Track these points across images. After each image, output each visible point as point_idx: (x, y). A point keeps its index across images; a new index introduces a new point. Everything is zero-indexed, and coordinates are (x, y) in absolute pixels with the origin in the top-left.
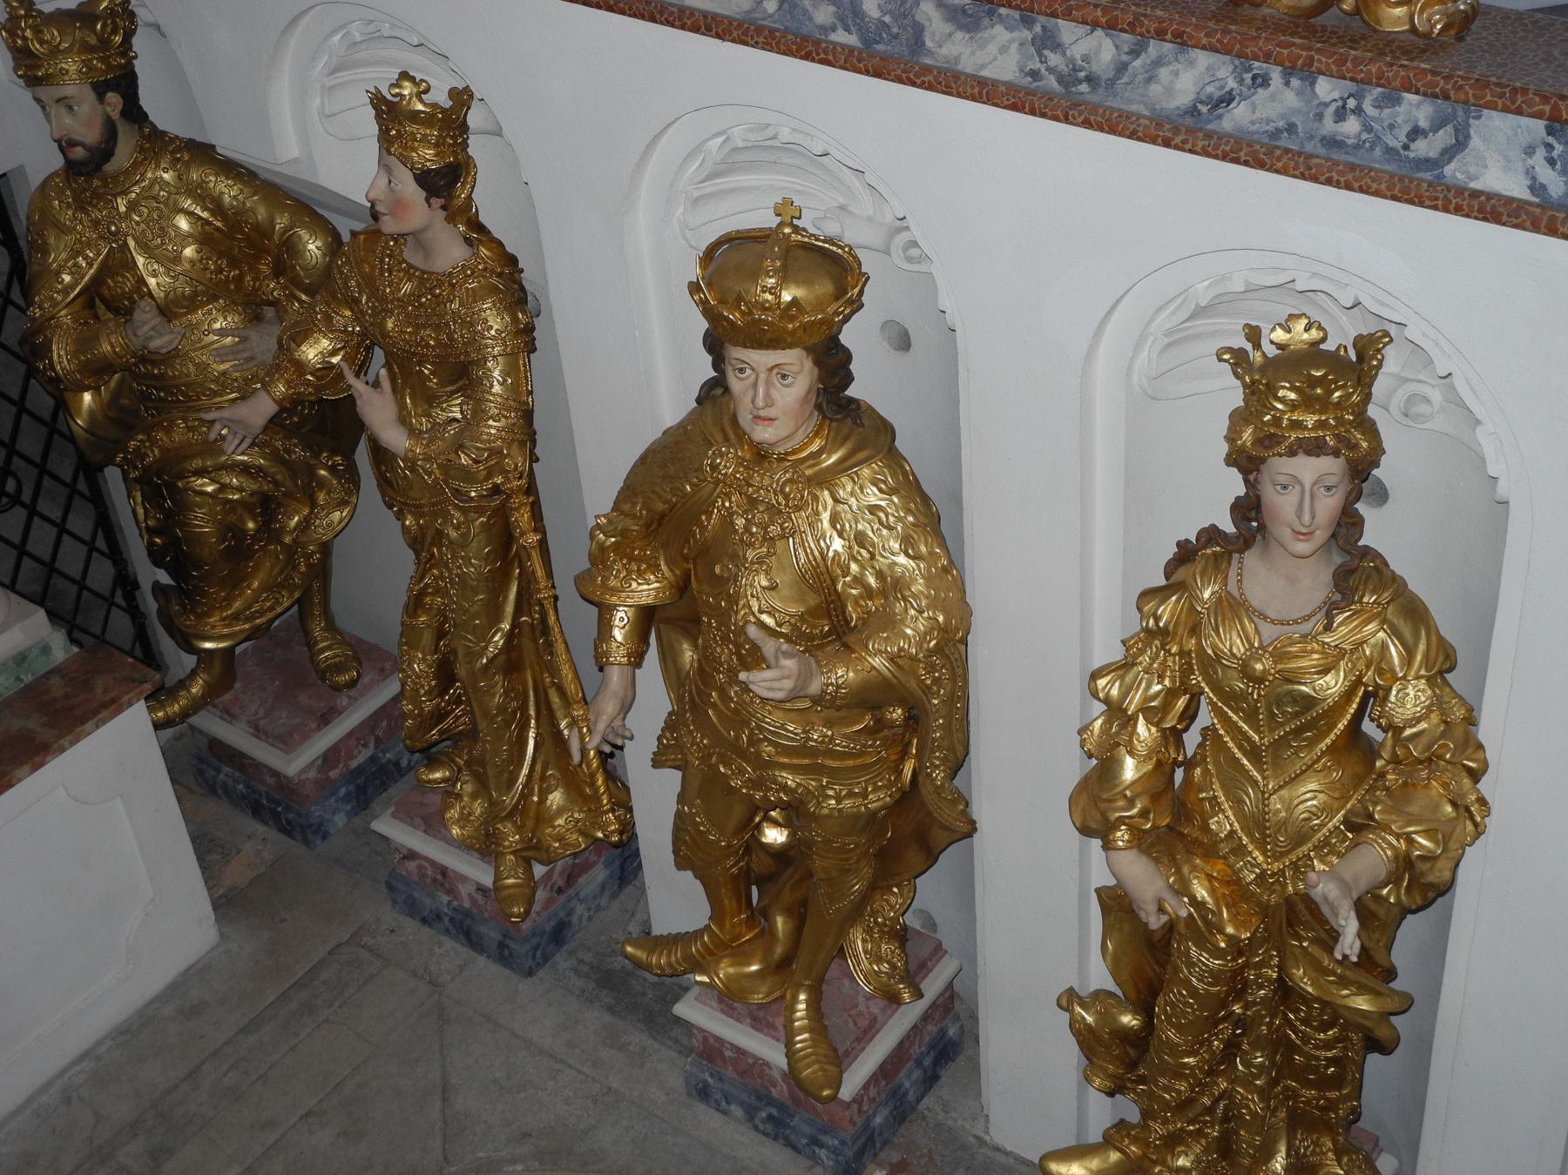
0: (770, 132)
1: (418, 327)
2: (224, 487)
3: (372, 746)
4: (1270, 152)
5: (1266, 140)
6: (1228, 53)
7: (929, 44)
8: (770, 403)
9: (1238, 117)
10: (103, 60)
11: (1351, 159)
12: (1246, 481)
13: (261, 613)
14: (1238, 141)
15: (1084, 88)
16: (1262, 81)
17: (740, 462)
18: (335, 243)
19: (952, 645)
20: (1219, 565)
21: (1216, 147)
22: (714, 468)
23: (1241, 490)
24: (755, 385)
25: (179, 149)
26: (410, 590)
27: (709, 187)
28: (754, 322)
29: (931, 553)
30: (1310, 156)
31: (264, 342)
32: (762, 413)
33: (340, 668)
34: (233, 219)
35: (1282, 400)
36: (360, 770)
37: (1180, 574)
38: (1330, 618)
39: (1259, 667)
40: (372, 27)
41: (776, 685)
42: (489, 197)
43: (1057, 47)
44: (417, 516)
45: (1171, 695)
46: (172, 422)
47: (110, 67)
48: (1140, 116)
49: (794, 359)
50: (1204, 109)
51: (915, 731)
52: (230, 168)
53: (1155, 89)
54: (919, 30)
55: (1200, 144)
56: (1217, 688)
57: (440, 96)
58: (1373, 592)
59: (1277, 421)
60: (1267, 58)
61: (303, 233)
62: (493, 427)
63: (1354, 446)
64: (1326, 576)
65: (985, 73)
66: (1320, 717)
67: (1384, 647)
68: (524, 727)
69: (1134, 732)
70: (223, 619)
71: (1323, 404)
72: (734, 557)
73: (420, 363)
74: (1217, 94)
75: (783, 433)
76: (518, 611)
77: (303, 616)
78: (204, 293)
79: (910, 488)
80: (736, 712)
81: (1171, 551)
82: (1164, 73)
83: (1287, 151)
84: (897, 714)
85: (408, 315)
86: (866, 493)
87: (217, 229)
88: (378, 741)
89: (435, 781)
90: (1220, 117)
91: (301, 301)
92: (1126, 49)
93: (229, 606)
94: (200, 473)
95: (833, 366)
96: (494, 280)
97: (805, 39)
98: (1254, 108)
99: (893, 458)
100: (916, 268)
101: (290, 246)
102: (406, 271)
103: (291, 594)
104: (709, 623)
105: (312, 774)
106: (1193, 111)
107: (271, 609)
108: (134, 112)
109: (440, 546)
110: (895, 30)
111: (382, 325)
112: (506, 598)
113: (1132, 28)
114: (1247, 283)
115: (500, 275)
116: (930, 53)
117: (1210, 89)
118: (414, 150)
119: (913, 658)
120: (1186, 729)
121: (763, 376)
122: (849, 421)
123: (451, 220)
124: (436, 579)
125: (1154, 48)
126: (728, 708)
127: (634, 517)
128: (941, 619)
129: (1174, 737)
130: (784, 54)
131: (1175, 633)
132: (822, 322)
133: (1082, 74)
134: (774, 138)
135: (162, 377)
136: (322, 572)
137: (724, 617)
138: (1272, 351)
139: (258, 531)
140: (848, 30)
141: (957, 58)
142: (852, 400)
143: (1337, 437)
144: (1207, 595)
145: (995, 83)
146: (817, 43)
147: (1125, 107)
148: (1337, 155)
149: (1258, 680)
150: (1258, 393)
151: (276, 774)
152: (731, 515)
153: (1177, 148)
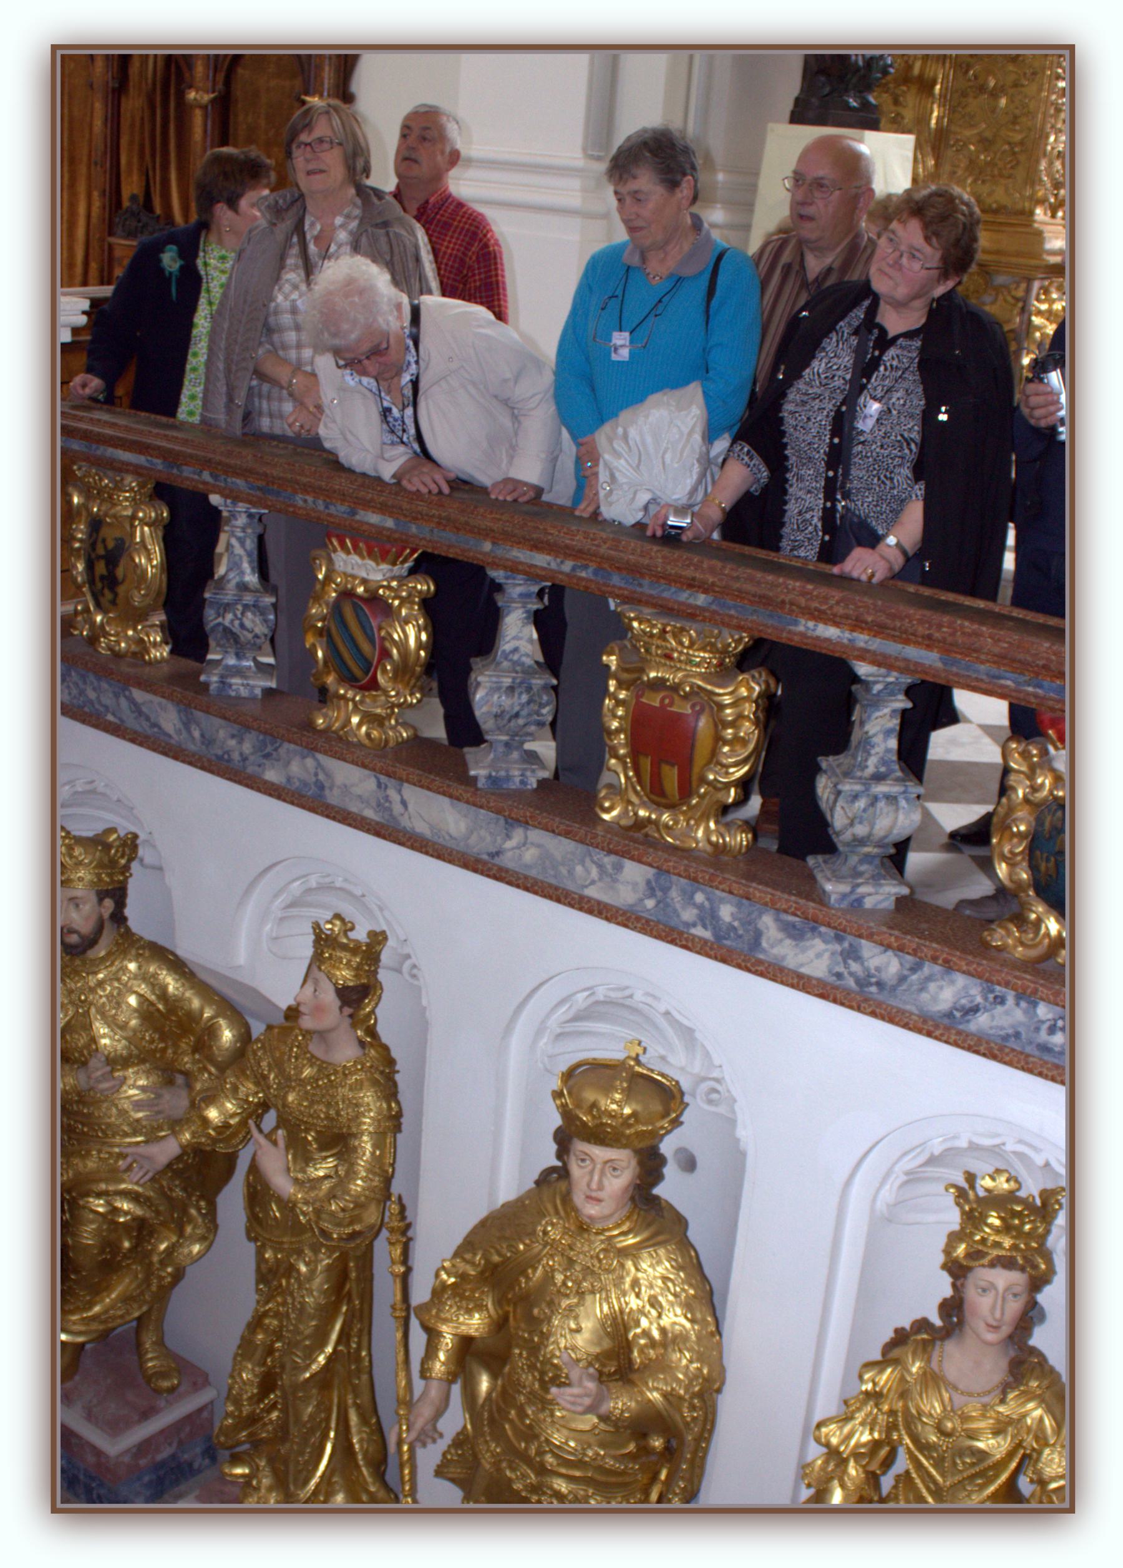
0: (627, 993)
1: (312, 1103)
2: (116, 1211)
3: (175, 1445)
4: (1001, 1049)
5: (999, 1041)
6: (980, 977)
7: (764, 944)
8: (601, 1187)
9: (982, 1022)
10: (110, 875)
11: (1056, 1061)
12: (954, 1285)
13: (114, 1318)
14: (980, 1039)
15: (873, 989)
16: (1000, 1000)
17: (566, 1232)
18: (245, 1037)
19: (708, 1390)
20: (926, 1348)
21: (964, 1041)
22: (545, 1233)
23: (948, 1292)
24: (592, 1172)
25: (143, 947)
26: (257, 1310)
27: (570, 1027)
28: (602, 1124)
29: (704, 1320)
30: (1028, 1056)
31: (177, 1102)
32: (594, 1194)
33: (164, 1375)
34: (173, 1004)
35: (990, 1226)
36: (163, 1463)
37: (895, 1353)
38: (1004, 1393)
39: (949, 1425)
40: (327, 880)
41: (579, 1400)
42: (389, 1015)
43: (858, 958)
44: (276, 1251)
45: (876, 1445)
46: (88, 1153)
47: (113, 881)
48: (911, 1014)
49: (622, 1156)
50: (958, 1014)
51: (669, 1461)
52: (178, 966)
53: (925, 996)
54: (758, 935)
55: (953, 1037)
56: (915, 1439)
57: (360, 934)
58: (1037, 1378)
59: (984, 1241)
60: (1007, 984)
61: (222, 1022)
62: (358, 1185)
63: (1035, 1267)
64: (1004, 1364)
65: (803, 970)
66: (990, 1468)
67: (1041, 1420)
68: (325, 1437)
69: (845, 1472)
70: (83, 1319)
71: (1019, 1233)
72: (551, 1304)
73: (307, 1131)
74: (968, 1005)
75: (607, 1212)
76: (338, 1342)
77: (138, 1331)
78: (138, 1057)
79: (693, 1267)
80: (530, 1427)
81: (888, 1335)
82: (932, 986)
83: (1013, 1050)
84: (657, 1443)
85: (307, 1092)
86: (654, 1270)
87: (158, 1010)
88: (181, 1443)
89: (236, 1476)
90: (968, 1021)
91: (210, 1073)
92: (908, 966)
93: (90, 1308)
94: (99, 1195)
95: (651, 1164)
96: (377, 1076)
97: (673, 929)
98: (993, 1017)
99: (685, 1245)
100: (713, 1109)
101: (212, 1031)
102: (309, 1060)
103: (140, 1307)
104: (520, 1354)
105: (127, 1459)
106: (949, 1015)
107: (122, 1317)
108: (118, 917)
109: (288, 1278)
110: (741, 932)
111: (285, 1098)
112: (333, 1327)
113: (915, 953)
114: (971, 1143)
115: (382, 1073)
116: (764, 951)
117: (963, 1001)
118: (339, 969)
119: (681, 1398)
120: (884, 1473)
121: (599, 1166)
122: (653, 1213)
123: (354, 1026)
124: (278, 1304)
125: (928, 968)
126: (523, 1423)
127: (473, 1264)
128: (705, 1371)
129: (873, 1479)
130: (656, 937)
131: (887, 1396)
132: (650, 1132)
133: (874, 980)
134: (631, 996)
135: (90, 1115)
136: (163, 1295)
137: (534, 1350)
138: (982, 1193)
139: (130, 1250)
140: (705, 927)
141: (784, 958)
142: (657, 1198)
143: (1024, 1258)
144: (914, 1370)
145: (809, 978)
146: (681, 933)
147: (901, 1006)
148: (1047, 1057)
149: (948, 1435)
150: (973, 1218)
151: (98, 1453)
152: (553, 1270)
153: (937, 1038)
